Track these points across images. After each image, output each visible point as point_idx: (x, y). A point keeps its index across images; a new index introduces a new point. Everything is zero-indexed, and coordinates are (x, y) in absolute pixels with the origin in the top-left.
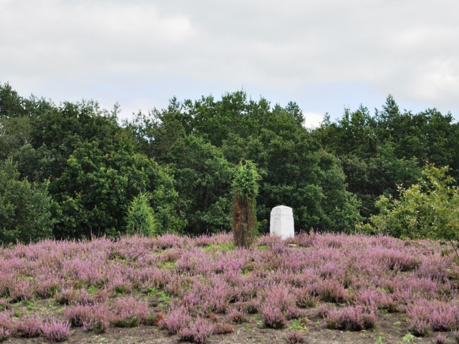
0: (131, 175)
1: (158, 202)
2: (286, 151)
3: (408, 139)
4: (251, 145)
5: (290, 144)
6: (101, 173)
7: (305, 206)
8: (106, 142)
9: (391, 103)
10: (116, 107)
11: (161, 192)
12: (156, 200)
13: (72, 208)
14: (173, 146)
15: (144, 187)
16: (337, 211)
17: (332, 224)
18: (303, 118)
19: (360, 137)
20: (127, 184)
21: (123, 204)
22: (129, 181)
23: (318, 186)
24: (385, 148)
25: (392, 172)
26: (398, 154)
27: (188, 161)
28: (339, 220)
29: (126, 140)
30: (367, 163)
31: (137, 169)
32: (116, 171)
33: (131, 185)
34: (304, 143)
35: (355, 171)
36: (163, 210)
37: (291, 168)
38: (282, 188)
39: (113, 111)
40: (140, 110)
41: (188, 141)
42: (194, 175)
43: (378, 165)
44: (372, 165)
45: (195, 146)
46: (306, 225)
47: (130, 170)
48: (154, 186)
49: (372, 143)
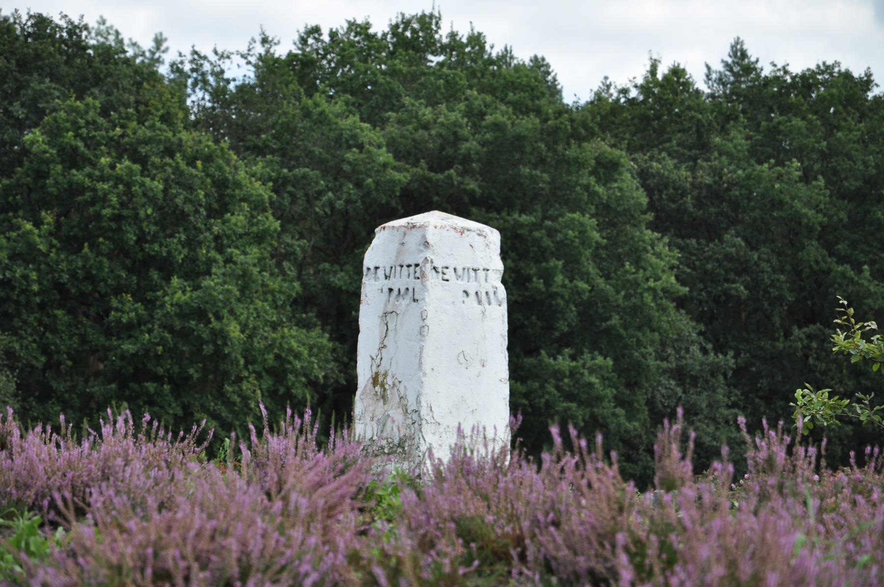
0: (173, 177)
1: (233, 241)
2: (520, 138)
3: (779, 123)
4: (442, 124)
5: (528, 123)
6: (102, 170)
7: (558, 259)
8: (120, 100)
9: (739, 53)
11: (242, 218)
13: (32, 246)
15: (201, 205)
16: (627, 272)
18: (559, 87)
20: (160, 196)
21: (152, 242)
22: (165, 191)
23: (588, 216)
24: (731, 140)
25: (744, 191)
26: (757, 154)
29: (168, 100)
30: (692, 169)
31: (188, 164)
32: (137, 167)
33: (171, 200)
34: (562, 123)
35: (666, 186)
36: (242, 257)
37: (532, 178)
38: (509, 218)
41: (308, 109)
42: (317, 183)
44: (702, 177)
45: (323, 120)
47: (170, 165)
48: (226, 204)
49: (703, 130)
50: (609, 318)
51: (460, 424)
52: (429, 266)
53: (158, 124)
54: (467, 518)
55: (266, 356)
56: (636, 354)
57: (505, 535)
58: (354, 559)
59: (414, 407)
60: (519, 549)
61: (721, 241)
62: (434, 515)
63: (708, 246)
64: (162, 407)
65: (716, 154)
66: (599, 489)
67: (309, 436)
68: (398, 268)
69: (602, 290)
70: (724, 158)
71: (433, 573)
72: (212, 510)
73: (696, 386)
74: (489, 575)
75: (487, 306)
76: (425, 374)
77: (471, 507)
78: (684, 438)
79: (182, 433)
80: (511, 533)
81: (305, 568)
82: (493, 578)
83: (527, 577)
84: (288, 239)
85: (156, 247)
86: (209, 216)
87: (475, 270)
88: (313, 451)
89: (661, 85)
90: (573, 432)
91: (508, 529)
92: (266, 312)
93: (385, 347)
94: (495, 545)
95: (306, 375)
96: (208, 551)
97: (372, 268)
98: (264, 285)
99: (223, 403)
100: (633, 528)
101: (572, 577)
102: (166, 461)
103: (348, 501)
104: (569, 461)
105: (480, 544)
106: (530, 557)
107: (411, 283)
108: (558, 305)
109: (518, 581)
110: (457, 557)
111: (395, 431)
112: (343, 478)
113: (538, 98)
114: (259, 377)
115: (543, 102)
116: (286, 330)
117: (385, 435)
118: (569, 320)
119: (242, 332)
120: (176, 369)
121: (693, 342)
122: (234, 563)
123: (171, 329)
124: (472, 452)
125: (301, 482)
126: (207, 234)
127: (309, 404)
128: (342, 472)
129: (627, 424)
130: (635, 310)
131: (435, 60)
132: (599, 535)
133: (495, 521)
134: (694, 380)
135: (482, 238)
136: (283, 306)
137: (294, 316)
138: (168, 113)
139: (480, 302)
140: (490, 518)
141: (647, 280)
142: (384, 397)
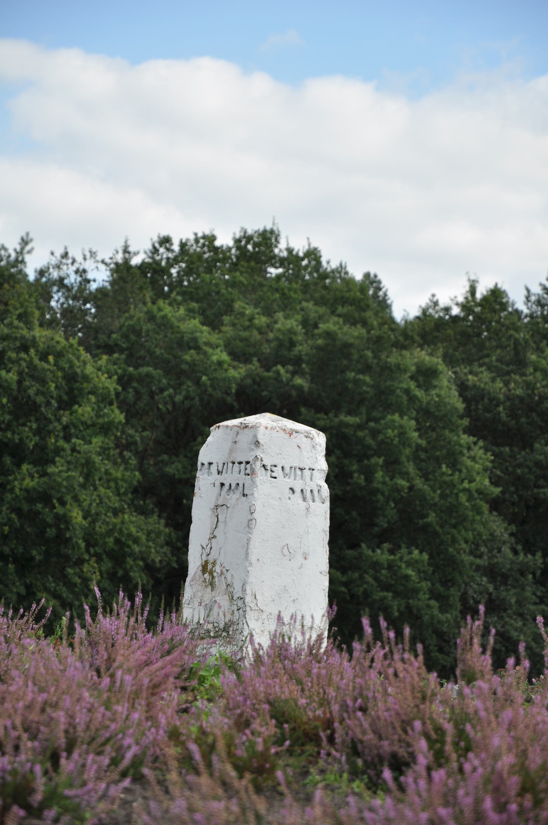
1: (80, 431)
2: (347, 346)
4: (279, 330)
5: (353, 334)
10: (25, 242)
11: (89, 409)
12: (75, 427)
14: (122, 320)
15: (52, 397)
16: (443, 474)
17: (433, 498)
18: (389, 302)
19: (497, 335)
20: (14, 386)
22: (20, 382)
27: (151, 353)
28: (448, 491)
30: (506, 384)
31: (41, 359)
33: (25, 391)
36: (86, 447)
37: (356, 382)
39: (18, 249)
40: (66, 248)
42: (160, 381)
43: (528, 389)
45: (165, 324)
46: (380, 497)
47: (25, 360)
48: (75, 397)
49: (520, 348)
50: (426, 516)
51: (280, 612)
52: (258, 464)
53: (16, 322)
54: (282, 701)
55: (107, 539)
56: (451, 550)
57: (316, 718)
58: (174, 735)
59: (240, 594)
60: (329, 732)
61: (532, 450)
62: (251, 696)
63: (520, 454)
64: (6, 586)
65: (531, 370)
66: (404, 678)
67: (140, 618)
68: (230, 465)
69: (420, 490)
70: (538, 375)
71: (247, 751)
72: (44, 684)
73: (506, 584)
74: (300, 755)
75: (311, 503)
76: (251, 564)
77: (285, 691)
78: (485, 633)
79: (22, 610)
80: (322, 715)
81: (128, 741)
82: (303, 757)
83: (335, 759)
84: (131, 432)
85: (9, 435)
86: (59, 408)
87: (301, 469)
88: (143, 632)
89: (480, 305)
90: (383, 624)
91: (319, 712)
92: (109, 498)
93: (215, 537)
94: (307, 726)
95: (143, 559)
96: (38, 723)
97: (206, 463)
98: (107, 473)
99: (65, 584)
100: (434, 716)
101: (376, 760)
102: (5, 636)
103: (172, 680)
104: (378, 652)
105: (293, 725)
106: (338, 740)
107: (242, 479)
108: (378, 501)
109: (326, 761)
110: (269, 737)
111: (220, 617)
112: (168, 658)
113: (364, 310)
114: (99, 559)
115: (368, 314)
116: (126, 516)
117: (211, 619)
118: (389, 517)
119: (85, 518)
120: (21, 549)
121: (504, 543)
122: (62, 735)
123: (19, 511)
124: (290, 639)
125: (128, 660)
126: (56, 424)
127: (140, 588)
128: (169, 652)
129: (440, 615)
130: (452, 510)
131: (273, 271)
132: (403, 721)
133: (308, 704)
134: (505, 578)
135: (309, 439)
136: (125, 494)
137: (133, 503)
138: (25, 312)
139: (304, 499)
140: (303, 701)
141: (462, 481)
142: (212, 585)
